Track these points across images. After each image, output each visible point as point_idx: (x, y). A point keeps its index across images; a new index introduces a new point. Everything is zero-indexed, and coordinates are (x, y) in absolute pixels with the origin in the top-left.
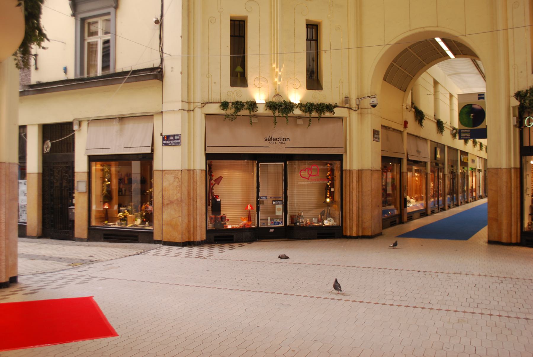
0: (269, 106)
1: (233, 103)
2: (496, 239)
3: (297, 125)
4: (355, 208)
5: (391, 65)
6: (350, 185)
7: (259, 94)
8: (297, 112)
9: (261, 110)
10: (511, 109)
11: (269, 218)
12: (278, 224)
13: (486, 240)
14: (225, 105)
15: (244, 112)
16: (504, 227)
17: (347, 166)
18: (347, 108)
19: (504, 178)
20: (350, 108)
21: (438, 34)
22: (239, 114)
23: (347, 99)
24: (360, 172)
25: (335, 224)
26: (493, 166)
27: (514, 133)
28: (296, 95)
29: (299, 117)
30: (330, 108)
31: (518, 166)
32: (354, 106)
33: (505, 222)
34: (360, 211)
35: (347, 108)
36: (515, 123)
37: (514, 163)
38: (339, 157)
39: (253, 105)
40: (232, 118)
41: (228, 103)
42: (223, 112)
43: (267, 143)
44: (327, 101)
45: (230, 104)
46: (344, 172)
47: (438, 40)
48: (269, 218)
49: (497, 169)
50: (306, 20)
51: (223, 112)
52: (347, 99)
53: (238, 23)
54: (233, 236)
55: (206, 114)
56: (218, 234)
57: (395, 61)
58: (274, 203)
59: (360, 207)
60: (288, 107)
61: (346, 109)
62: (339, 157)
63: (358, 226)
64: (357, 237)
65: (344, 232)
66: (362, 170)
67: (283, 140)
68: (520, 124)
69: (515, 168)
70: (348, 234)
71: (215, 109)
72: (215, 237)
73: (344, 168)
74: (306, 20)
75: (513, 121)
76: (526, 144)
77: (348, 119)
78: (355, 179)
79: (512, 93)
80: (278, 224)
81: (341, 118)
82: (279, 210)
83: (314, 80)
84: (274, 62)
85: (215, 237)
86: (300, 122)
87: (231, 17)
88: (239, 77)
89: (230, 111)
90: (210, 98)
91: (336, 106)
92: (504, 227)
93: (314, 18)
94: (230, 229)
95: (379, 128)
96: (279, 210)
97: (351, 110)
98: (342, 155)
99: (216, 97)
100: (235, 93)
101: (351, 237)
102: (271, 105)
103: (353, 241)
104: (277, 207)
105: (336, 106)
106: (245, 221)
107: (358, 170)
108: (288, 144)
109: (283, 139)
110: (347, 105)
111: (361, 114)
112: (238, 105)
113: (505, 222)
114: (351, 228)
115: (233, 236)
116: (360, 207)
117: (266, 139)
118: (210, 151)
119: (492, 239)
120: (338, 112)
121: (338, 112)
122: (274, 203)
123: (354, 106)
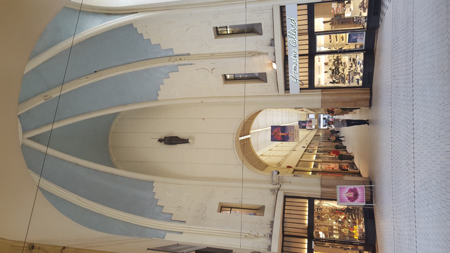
2: (369, 102)
5: (254, 166)
13: (368, 108)
16: (359, 97)
19: (327, 97)
20: (278, 189)
21: (237, 138)
23: (272, 190)
24: (322, 186)
26: (320, 104)
31: (321, 90)
37: (319, 92)
47: (240, 139)
49: (322, 102)
52: (272, 190)
57: (252, 164)
61: (279, 192)
66: (321, 185)
69: (322, 91)
70: (370, 197)
73: (320, 197)
76: (307, 86)
94: (363, 74)
95: (293, 174)
97: (280, 189)
103: (374, 97)
106: (343, 57)
107: (321, 187)
110: (276, 191)
119: (368, 104)
123: (277, 186)
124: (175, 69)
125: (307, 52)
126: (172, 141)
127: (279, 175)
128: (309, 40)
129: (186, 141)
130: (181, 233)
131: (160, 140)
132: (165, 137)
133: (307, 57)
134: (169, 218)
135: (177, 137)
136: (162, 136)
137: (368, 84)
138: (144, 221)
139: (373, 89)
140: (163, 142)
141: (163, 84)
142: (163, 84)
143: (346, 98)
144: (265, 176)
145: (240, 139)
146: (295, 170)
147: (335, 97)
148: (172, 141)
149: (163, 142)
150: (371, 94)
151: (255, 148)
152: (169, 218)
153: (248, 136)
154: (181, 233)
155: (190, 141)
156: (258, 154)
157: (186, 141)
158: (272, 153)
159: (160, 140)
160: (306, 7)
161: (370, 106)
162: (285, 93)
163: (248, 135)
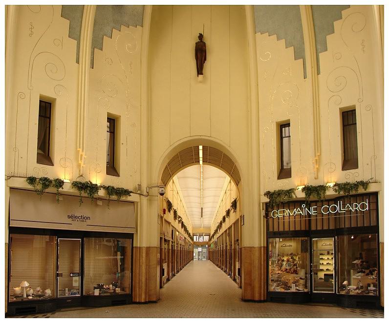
0: (75, 185)
1: (41, 179)
3: (97, 205)
4: (144, 280)
5: (166, 167)
6: (139, 260)
7: (64, 172)
8: (101, 193)
9: (67, 188)
10: (261, 204)
11: (67, 289)
12: (75, 294)
14: (32, 180)
15: (52, 189)
16: (257, 290)
17: (137, 243)
18: (139, 194)
19: (257, 254)
20: (140, 194)
22: (47, 190)
24: (148, 249)
25: (306, 290)
27: (263, 221)
28: (98, 178)
29: (100, 199)
30: (127, 192)
31: (266, 246)
32: (145, 193)
33: (257, 285)
34: (148, 281)
35: (139, 194)
36: (264, 215)
38: (130, 236)
39: (60, 183)
40: (40, 193)
41: (36, 179)
42: (30, 187)
43: (70, 221)
44: (125, 187)
45: (38, 180)
46: (134, 248)
47: (201, 147)
48: (67, 289)
50: (108, 114)
51: (30, 187)
53: (44, 104)
54: (35, 308)
55: (11, 188)
56: (20, 307)
57: (169, 164)
58: (71, 275)
59: (148, 278)
60: (93, 188)
62: (130, 236)
63: (146, 294)
64: (145, 303)
65: (133, 299)
67: (84, 219)
68: (267, 215)
69: (264, 247)
70: (138, 301)
71: (21, 183)
72: (17, 309)
73: (134, 246)
74: (108, 114)
75: (263, 213)
76: (271, 230)
77: (139, 203)
78: (144, 255)
79: (262, 193)
80: (75, 294)
81: (133, 202)
82: (76, 281)
83: (112, 168)
84: (80, 148)
85: (17, 309)
86: (100, 203)
87: (41, 97)
88: (45, 154)
89: (39, 187)
90: (16, 172)
91: (131, 192)
92: (257, 290)
93: (114, 112)
96: (76, 281)
97: (142, 196)
98: (133, 234)
99: (22, 171)
100: (41, 170)
101: (140, 303)
102: (76, 184)
103: (257, 305)
104: (74, 278)
105: (131, 192)
108: (89, 222)
109: (84, 218)
110: (139, 192)
111: (150, 200)
112: (46, 182)
113: (257, 285)
114: (140, 296)
115: (35, 308)
116: (148, 278)
117: (69, 217)
118: (13, 224)
120: (133, 197)
121: (133, 197)
122: (71, 275)
123: (145, 193)
124: (299, 54)
125: (313, 228)
126: (201, 53)
127: (159, 195)
128: (364, 227)
129: (200, 71)
130: (78, 62)
131: (201, 37)
132: (205, 44)
133: (307, 229)
134: (97, 44)
135: (205, 59)
136: (207, 41)
137: (271, 298)
138: (90, 12)
139: (266, 303)
140: (198, 40)
141: (278, 39)
142: (278, 39)
143: (256, 275)
144: (157, 179)
145: (201, 147)
146: (162, 217)
147: (256, 262)
148: (201, 53)
149: (198, 40)
150: (260, 301)
151: (180, 174)
152: (97, 44)
153: (201, 162)
154: (78, 62)
155: (200, 76)
156: (175, 178)
157: (200, 71)
158: (175, 193)
159: (201, 37)
160: (373, 224)
161: (245, 300)
162: (263, 203)
163: (203, 162)
